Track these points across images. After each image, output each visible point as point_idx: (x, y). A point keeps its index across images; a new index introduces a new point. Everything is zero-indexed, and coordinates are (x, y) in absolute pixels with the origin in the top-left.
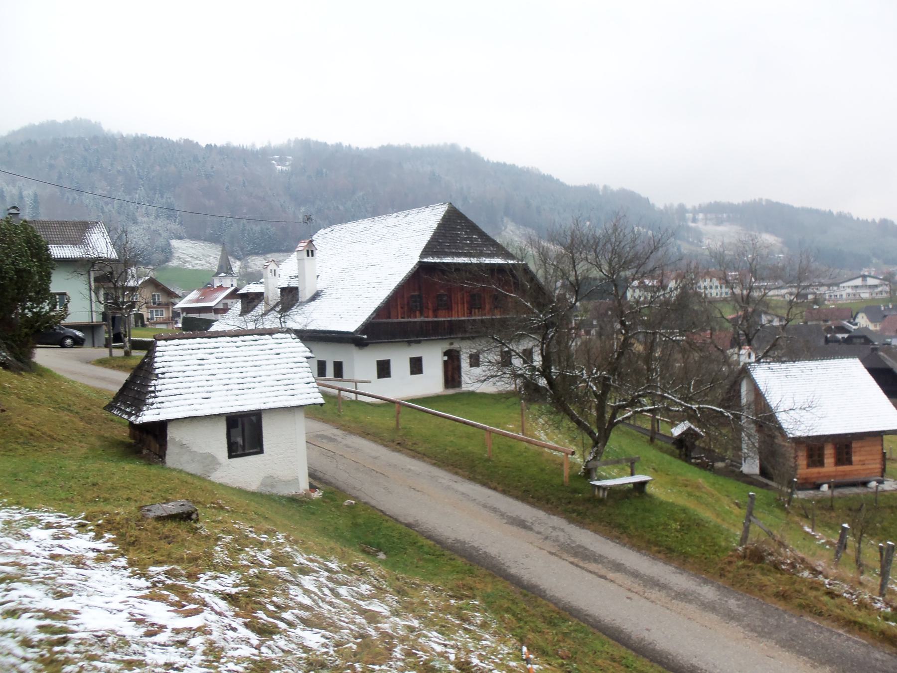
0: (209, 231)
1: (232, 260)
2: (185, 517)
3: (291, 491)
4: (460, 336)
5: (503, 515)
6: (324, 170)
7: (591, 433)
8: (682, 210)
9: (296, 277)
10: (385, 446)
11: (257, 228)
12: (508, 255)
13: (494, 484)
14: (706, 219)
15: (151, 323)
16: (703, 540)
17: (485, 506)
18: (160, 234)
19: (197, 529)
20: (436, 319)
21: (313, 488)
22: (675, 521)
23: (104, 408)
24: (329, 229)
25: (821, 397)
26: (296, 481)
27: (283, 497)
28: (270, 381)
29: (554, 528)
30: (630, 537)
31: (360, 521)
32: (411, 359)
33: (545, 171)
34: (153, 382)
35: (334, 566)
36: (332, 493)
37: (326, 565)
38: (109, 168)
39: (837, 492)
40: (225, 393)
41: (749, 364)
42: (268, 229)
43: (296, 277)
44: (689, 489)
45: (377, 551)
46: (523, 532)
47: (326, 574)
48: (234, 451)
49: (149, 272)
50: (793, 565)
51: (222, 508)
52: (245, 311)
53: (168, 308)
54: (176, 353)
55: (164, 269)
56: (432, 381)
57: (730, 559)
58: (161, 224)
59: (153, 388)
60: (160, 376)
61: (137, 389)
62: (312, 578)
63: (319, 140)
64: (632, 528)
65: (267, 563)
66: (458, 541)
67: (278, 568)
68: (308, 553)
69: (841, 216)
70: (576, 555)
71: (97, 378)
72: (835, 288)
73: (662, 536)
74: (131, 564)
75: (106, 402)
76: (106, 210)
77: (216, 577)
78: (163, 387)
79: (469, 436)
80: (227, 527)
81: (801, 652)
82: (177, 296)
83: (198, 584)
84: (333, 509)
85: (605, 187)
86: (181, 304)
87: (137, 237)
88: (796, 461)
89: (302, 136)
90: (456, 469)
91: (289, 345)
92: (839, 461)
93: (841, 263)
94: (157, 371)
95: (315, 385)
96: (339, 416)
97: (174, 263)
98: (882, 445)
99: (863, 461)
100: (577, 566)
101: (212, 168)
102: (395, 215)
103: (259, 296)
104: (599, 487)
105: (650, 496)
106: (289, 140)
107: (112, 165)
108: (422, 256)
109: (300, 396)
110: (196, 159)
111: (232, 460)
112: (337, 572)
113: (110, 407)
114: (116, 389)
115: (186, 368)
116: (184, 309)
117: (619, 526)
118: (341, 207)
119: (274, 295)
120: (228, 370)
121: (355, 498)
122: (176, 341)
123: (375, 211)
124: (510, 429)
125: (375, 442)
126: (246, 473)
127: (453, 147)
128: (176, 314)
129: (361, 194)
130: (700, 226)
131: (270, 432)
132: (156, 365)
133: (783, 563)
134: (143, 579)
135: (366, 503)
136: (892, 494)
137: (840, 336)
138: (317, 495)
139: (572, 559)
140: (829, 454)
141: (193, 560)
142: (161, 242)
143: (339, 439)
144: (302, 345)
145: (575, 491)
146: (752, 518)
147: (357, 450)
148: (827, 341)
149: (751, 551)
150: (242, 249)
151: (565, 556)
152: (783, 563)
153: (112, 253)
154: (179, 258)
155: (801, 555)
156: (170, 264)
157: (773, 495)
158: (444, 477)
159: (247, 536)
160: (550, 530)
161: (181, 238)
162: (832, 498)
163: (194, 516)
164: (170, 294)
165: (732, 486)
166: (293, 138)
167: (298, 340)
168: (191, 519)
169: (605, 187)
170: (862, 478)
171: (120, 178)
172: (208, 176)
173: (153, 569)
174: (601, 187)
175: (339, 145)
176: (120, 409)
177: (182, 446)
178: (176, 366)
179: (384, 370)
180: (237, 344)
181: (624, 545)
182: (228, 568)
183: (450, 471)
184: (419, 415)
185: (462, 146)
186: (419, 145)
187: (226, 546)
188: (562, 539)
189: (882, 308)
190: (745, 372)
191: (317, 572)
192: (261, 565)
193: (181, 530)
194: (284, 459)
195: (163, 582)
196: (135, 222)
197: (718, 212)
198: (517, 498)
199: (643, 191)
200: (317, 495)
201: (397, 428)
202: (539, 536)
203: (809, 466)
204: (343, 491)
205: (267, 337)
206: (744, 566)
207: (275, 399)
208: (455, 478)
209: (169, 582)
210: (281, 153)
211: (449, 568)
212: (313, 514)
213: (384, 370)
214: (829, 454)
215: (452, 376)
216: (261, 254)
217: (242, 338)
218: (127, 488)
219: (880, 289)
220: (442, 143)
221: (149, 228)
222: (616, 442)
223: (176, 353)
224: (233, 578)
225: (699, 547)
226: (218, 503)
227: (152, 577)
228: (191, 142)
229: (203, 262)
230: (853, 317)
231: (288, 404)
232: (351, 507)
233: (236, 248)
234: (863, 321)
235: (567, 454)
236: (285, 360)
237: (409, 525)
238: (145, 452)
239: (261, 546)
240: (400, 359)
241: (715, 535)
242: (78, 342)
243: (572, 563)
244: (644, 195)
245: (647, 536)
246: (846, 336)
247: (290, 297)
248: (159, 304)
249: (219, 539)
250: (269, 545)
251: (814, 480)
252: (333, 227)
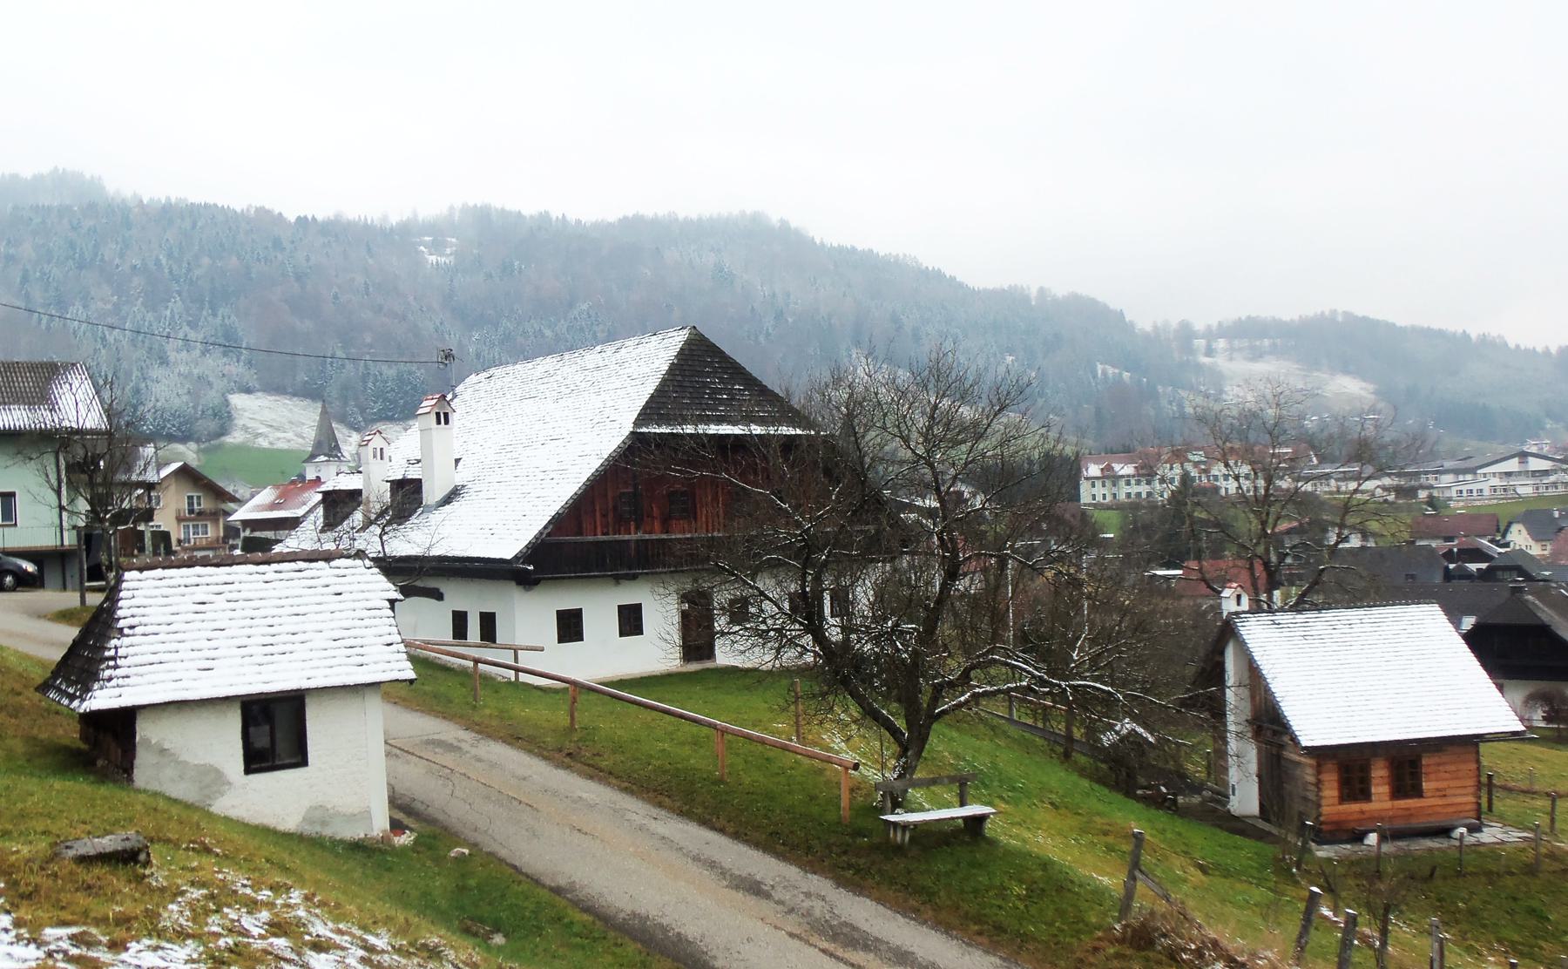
0: (302, 377)
1: (340, 431)
2: (128, 858)
3: (355, 832)
5: (723, 873)
7: (895, 732)
8: (1186, 334)
10: (545, 758)
11: (390, 372)
12: (795, 417)
13: (722, 822)
14: (1232, 349)
15: (185, 549)
16: (1061, 913)
17: (696, 859)
18: (210, 384)
19: (144, 876)
20: (664, 536)
21: (397, 827)
22: (1021, 881)
23: (37, 689)
24: (486, 374)
25: (1372, 675)
26: (366, 815)
27: (341, 841)
28: (320, 641)
29: (808, 895)
30: (937, 909)
31: (472, 882)
32: (620, 607)
33: (929, 261)
34: (113, 642)
35: (380, 943)
36: (435, 837)
37: (365, 941)
38: (117, 261)
39: (1387, 848)
40: (240, 661)
41: (1237, 614)
42: (410, 373)
44: (1110, 839)
45: (492, 932)
46: (752, 901)
47: (361, 953)
48: (257, 760)
49: (188, 453)
50: (1199, 953)
51: (207, 850)
52: (330, 524)
53: (217, 521)
54: (157, 592)
55: (220, 447)
56: (657, 650)
57: (1097, 944)
58: (214, 364)
59: (112, 653)
60: (126, 631)
61: (85, 660)
62: (332, 957)
63: (508, 208)
64: (942, 893)
65: (256, 931)
66: (634, 915)
67: (272, 940)
68: (337, 920)
69: (1484, 341)
70: (834, 938)
71: (53, 644)
72: (1469, 477)
73: (992, 906)
74: (18, 924)
75: (39, 681)
76: (111, 339)
77: (156, 949)
78: (131, 650)
79: (695, 743)
80: (202, 875)
82: (234, 499)
83: (124, 956)
84: (429, 863)
85: (1042, 290)
86: (242, 514)
87: (165, 391)
88: (1319, 790)
89: (476, 199)
90: (660, 798)
91: (359, 578)
92: (1398, 792)
93: (1487, 427)
94: (121, 624)
95: (402, 647)
96: (474, 707)
97: (235, 438)
98: (1478, 761)
99: (1443, 792)
100: (831, 955)
101: (308, 259)
102: (598, 348)
103: (354, 496)
104: (895, 824)
105: (992, 843)
106: (451, 208)
107: (122, 256)
108: (637, 423)
109: (372, 667)
110: (277, 244)
111: (251, 777)
112: (383, 951)
113: (44, 687)
114: (57, 655)
115: (173, 618)
116: (246, 523)
117: (920, 891)
118: (548, 333)
119: (378, 491)
120: (248, 622)
121: (474, 846)
122: (159, 572)
123: (611, 337)
124: (779, 730)
125: (530, 752)
126: (276, 800)
128: (232, 532)
129: (585, 307)
130: (1221, 362)
131: (319, 727)
132: (120, 613)
133: (1185, 950)
134: (32, 946)
135: (490, 854)
136: (1493, 851)
137: (1473, 567)
138: (405, 839)
139: (825, 945)
140: (1379, 773)
141: (124, 921)
142: (211, 397)
143: (465, 747)
144: (383, 578)
145: (859, 833)
146: (1137, 874)
147: (493, 765)
148: (1448, 576)
149: (1134, 930)
150: (363, 411)
151: (815, 939)
152: (1185, 950)
153: (93, 419)
154: (245, 429)
155: (1213, 935)
156: (228, 439)
157: (1270, 850)
158: (637, 809)
159: (235, 892)
160: (802, 896)
161: (248, 391)
162: (1379, 858)
163: (142, 857)
164: (220, 495)
165: (1202, 839)
166: (458, 205)
167: (376, 570)
168: (136, 862)
169: (1042, 290)
170: (1445, 823)
171: (136, 281)
172: (298, 278)
173: (50, 932)
174: (1034, 292)
175: (544, 217)
176: (59, 690)
177: (163, 751)
178: (155, 615)
179: (570, 627)
180: (266, 578)
181: (924, 922)
182: (181, 935)
183: (649, 801)
184: (619, 706)
185: (775, 218)
186: (694, 216)
187: (191, 905)
188: (817, 913)
189: (1556, 514)
190: (1228, 631)
191: (343, 949)
192: (245, 933)
193: (117, 880)
194: (347, 779)
195: (65, 952)
196: (164, 361)
197: (1251, 335)
198: (757, 845)
199: (1110, 295)
200: (405, 839)
201: (572, 729)
202: (779, 908)
203: (1343, 799)
204: (456, 835)
205: (321, 564)
206: (1118, 956)
207: (328, 671)
208: (655, 811)
209: (74, 951)
210: (437, 232)
211: (610, 958)
212: (389, 870)
213: (570, 627)
214: (1379, 773)
215: (697, 642)
216: (399, 419)
217: (275, 566)
218: (49, 816)
219: (1552, 478)
220: (736, 212)
221: (190, 373)
222: (943, 744)
223: (157, 592)
224: (187, 951)
225: (1050, 924)
226: (203, 843)
227: (48, 943)
228: (268, 212)
229: (290, 435)
230: (1499, 530)
231: (351, 681)
232: (461, 859)
233: (351, 407)
234: (1519, 538)
235: (847, 769)
236: (353, 605)
237: (557, 891)
238: (100, 763)
239: (253, 906)
240: (599, 608)
241: (1084, 905)
242: (25, 582)
243: (824, 951)
244: (1114, 305)
245: (965, 907)
246: (1484, 566)
247: (407, 497)
248: (200, 513)
249: (183, 893)
250: (270, 905)
251: (1352, 825)
252: (492, 371)
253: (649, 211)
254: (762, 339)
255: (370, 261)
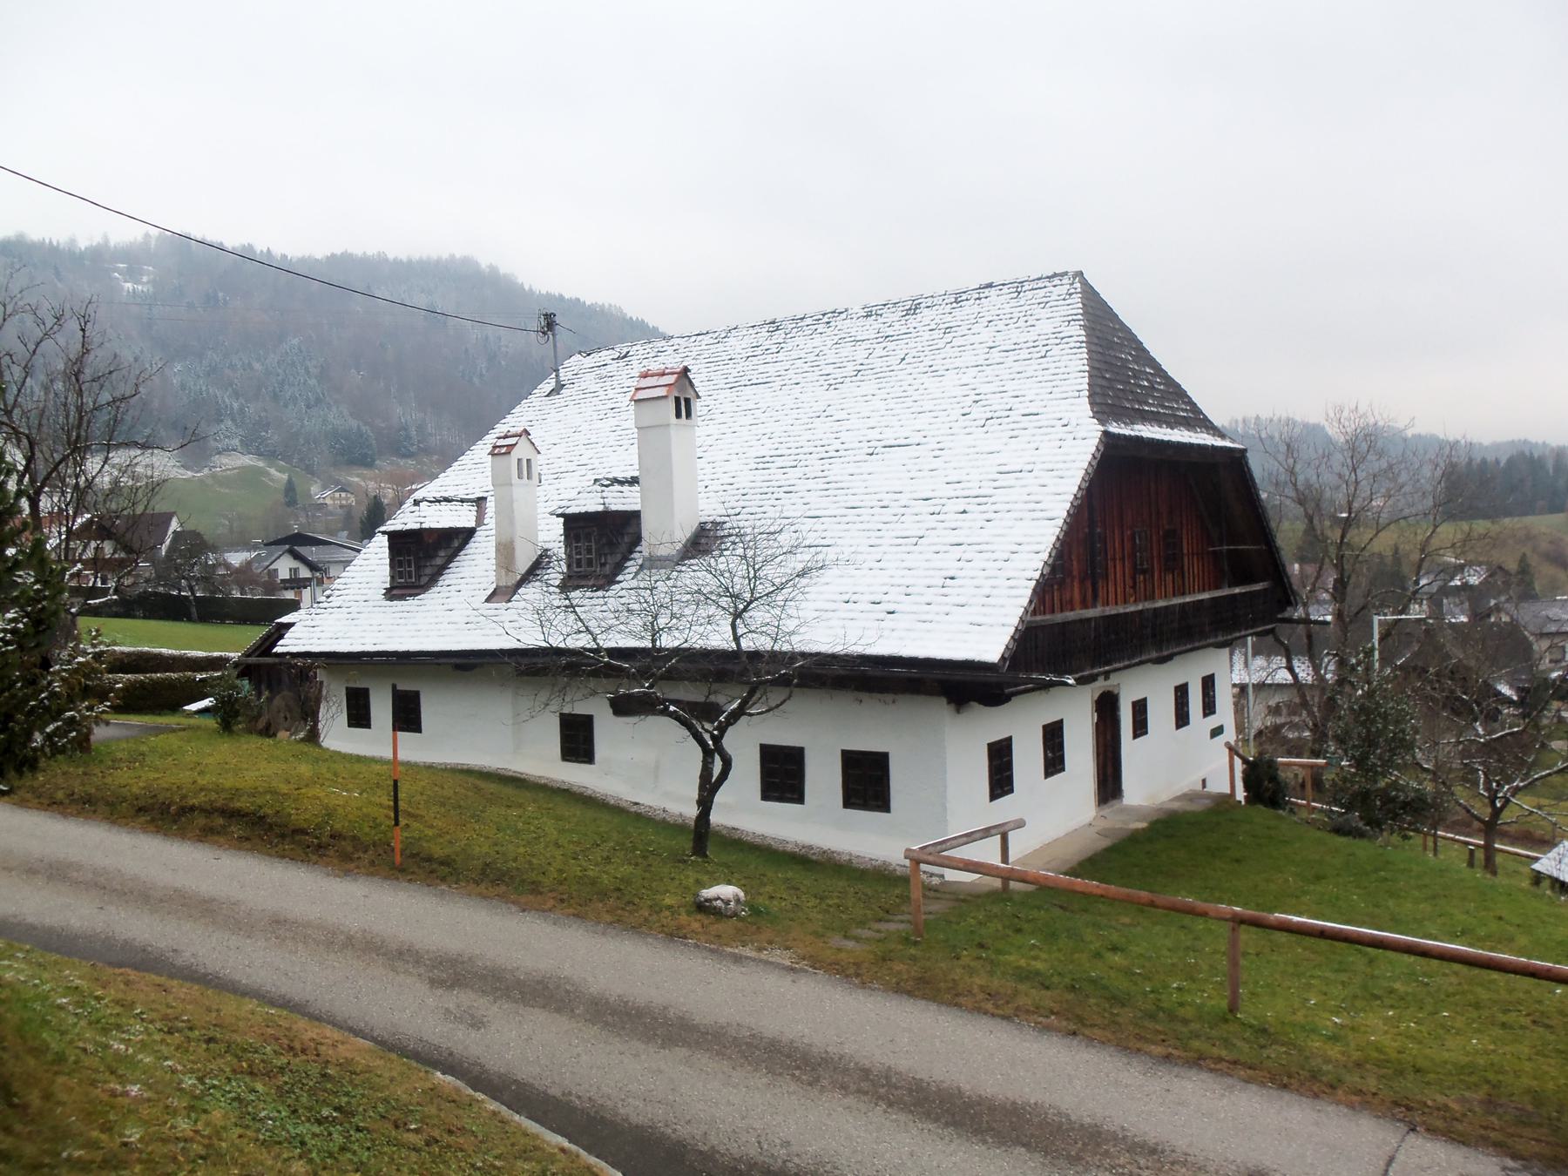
4: (1154, 655)
6: (220, 294)
9: (634, 481)
10: (1198, 1061)
12: (1223, 436)
43: (634, 481)
81: (928, 1115)
118: (257, 366)
127: (467, 262)
129: (295, 341)
184: (1352, 955)
185: (484, 262)
186: (403, 257)
210: (133, 258)
220: (445, 256)
253: (357, 251)
254: (476, 380)
255: (59, 285)
